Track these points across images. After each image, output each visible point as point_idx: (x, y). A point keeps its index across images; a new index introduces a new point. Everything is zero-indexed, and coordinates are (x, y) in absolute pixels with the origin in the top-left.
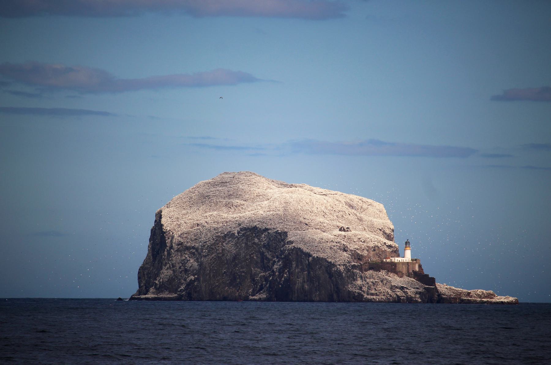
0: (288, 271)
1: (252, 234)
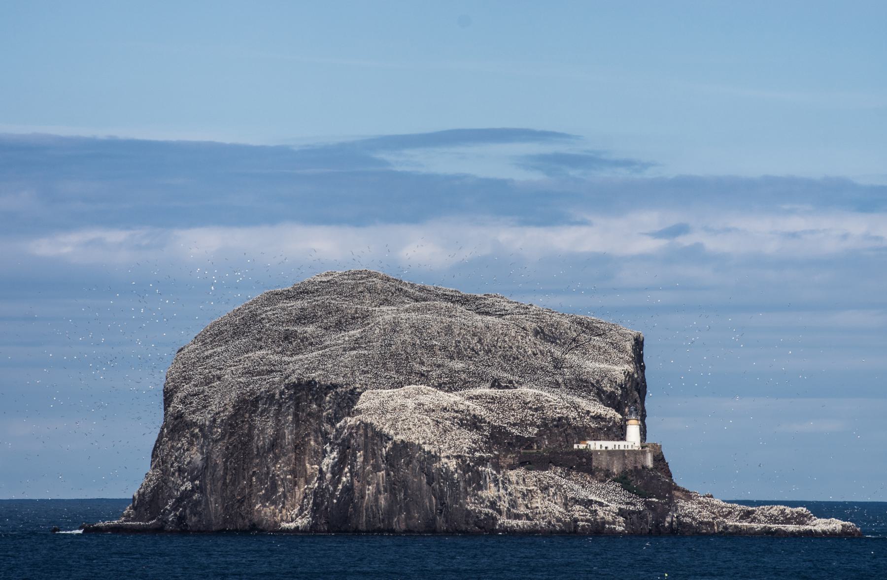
0: (350, 471)
1: (307, 395)
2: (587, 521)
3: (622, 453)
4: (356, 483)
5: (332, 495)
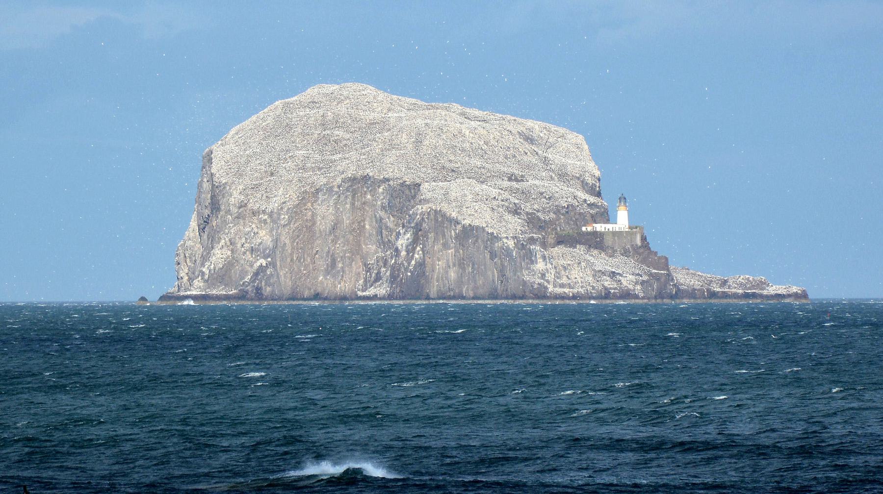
0: (422, 249)
1: (362, 187)
2: (615, 289)
3: (614, 234)
4: (428, 260)
5: (406, 269)
